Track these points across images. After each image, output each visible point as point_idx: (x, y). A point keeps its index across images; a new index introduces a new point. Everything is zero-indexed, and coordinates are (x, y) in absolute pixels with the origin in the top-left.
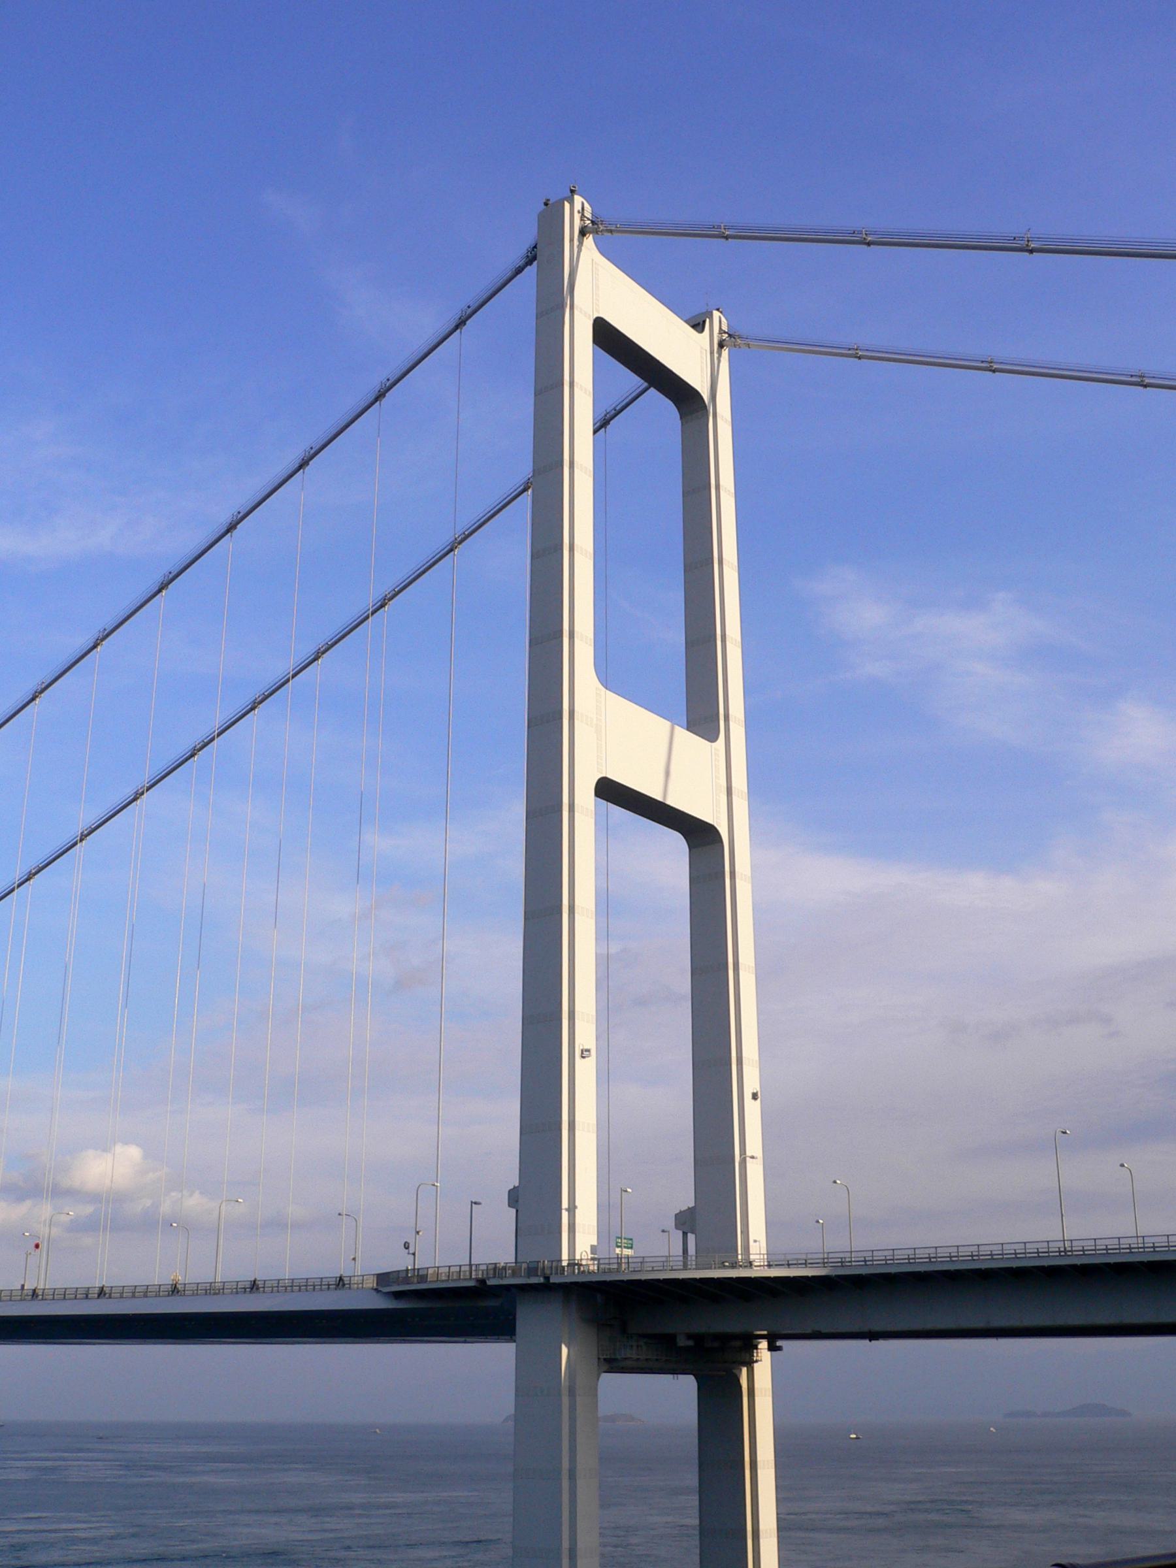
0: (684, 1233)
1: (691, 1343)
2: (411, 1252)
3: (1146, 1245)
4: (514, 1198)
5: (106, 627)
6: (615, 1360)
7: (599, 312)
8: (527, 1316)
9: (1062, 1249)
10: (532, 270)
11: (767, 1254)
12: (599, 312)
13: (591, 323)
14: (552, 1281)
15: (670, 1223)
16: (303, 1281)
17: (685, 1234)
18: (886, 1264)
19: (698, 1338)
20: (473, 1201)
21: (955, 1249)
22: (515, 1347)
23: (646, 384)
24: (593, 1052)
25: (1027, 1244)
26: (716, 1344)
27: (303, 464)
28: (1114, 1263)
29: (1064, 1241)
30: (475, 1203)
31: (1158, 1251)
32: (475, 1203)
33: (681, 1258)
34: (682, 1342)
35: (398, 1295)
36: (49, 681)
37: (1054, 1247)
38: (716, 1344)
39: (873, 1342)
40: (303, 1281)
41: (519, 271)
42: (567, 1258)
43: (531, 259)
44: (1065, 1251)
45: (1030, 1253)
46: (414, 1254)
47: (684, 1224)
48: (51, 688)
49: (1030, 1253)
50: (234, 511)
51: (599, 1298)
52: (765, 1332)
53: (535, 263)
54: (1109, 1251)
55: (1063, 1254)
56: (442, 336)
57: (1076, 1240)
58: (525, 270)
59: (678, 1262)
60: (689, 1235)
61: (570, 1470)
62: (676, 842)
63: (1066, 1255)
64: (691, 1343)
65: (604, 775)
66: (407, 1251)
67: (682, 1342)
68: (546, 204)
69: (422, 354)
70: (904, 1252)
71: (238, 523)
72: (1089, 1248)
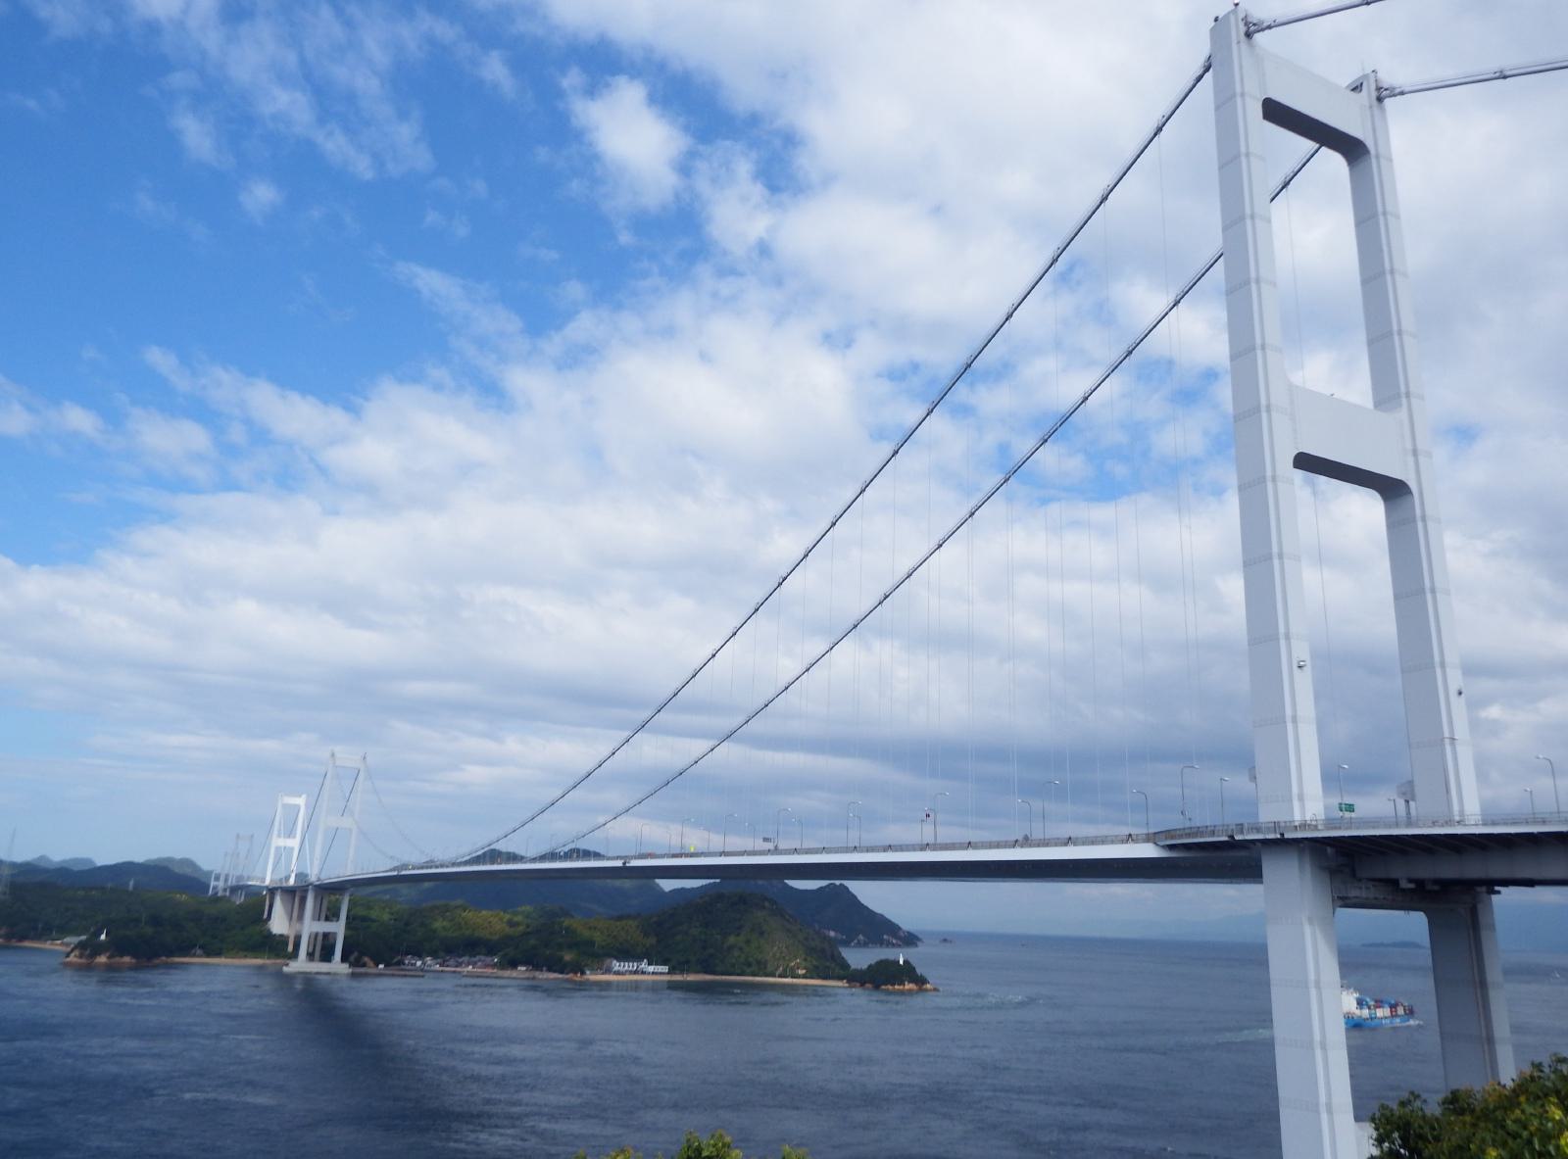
1: (1412, 886)
6: (1346, 898)
8: (1270, 866)
13: (1261, 103)
14: (1286, 836)
19: (1420, 883)
22: (1260, 814)
23: (1318, 145)
24: (1308, 663)
26: (1436, 888)
34: (1404, 884)
35: (1171, 847)
36: (1169, 113)
38: (1436, 888)
41: (1199, 79)
51: (1329, 850)
53: (1211, 70)
57: (1317, 151)
61: (1299, 796)
62: (1367, 507)
67: (1404, 884)
71: (1164, 125)
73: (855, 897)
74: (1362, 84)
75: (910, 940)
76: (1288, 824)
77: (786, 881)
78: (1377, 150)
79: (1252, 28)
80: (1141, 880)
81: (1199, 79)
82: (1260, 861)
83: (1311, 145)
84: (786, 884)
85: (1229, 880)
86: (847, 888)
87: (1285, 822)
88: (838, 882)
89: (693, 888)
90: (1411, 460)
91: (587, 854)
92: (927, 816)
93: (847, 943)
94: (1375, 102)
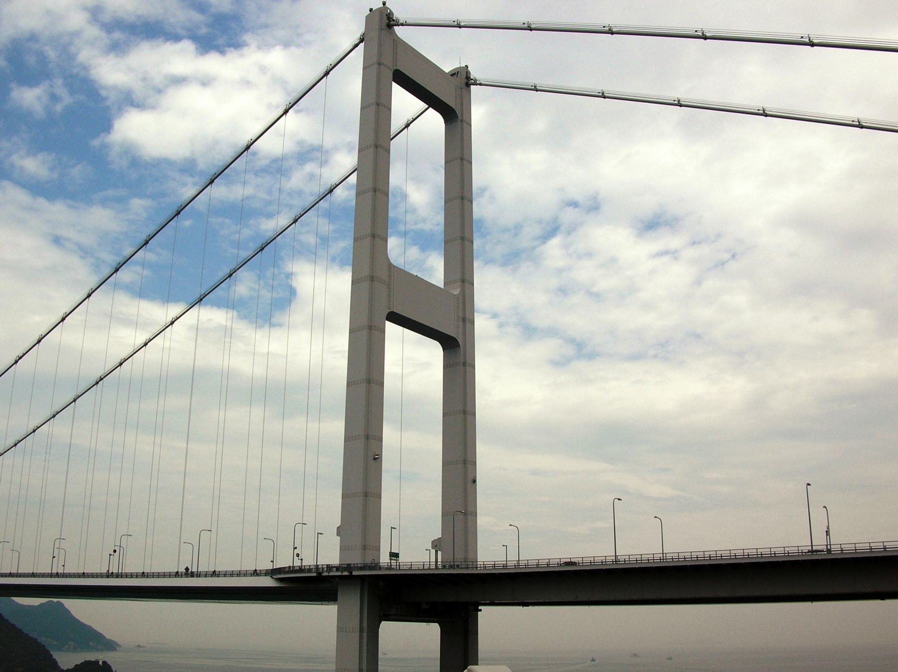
0: (436, 551)
2: (300, 558)
3: (732, 555)
4: (339, 532)
5: (252, 138)
7: (396, 67)
9: (614, 560)
10: (362, 45)
11: (441, 562)
12: (396, 67)
15: (429, 546)
16: (780, 549)
17: (436, 552)
18: (537, 567)
20: (393, 527)
21: (526, 562)
23: (427, 106)
25: (692, 553)
27: (89, 296)
28: (821, 559)
29: (663, 554)
30: (393, 528)
31: (723, 559)
32: (393, 528)
33: (434, 563)
35: (281, 580)
36: (69, 312)
37: (657, 557)
39: (524, 607)
40: (780, 549)
41: (356, 46)
42: (440, 561)
43: (361, 41)
44: (663, 559)
45: (834, 551)
46: (302, 560)
47: (436, 546)
48: (277, 122)
49: (834, 551)
50: (90, 288)
51: (381, 583)
52: (489, 602)
54: (750, 556)
55: (665, 560)
56: (277, 118)
58: (360, 45)
59: (433, 567)
60: (439, 552)
63: (561, 566)
64: (427, 607)
65: (392, 310)
66: (298, 558)
68: (370, 11)
69: (311, 85)
70: (544, 561)
72: (701, 556)
73: (70, 612)
74: (458, 72)
75: (111, 646)
76: (356, 565)
77: (12, 598)
78: (462, 116)
79: (392, 23)
80: (158, 600)
81: (356, 46)
82: (337, 591)
83: (422, 105)
84: (13, 600)
85: (327, 603)
86: (62, 605)
87: (354, 564)
88: (55, 600)
89: (75, 618)
90: (461, 323)
91: (305, 209)
92: (115, 551)
93: (59, 648)
94: (464, 86)
